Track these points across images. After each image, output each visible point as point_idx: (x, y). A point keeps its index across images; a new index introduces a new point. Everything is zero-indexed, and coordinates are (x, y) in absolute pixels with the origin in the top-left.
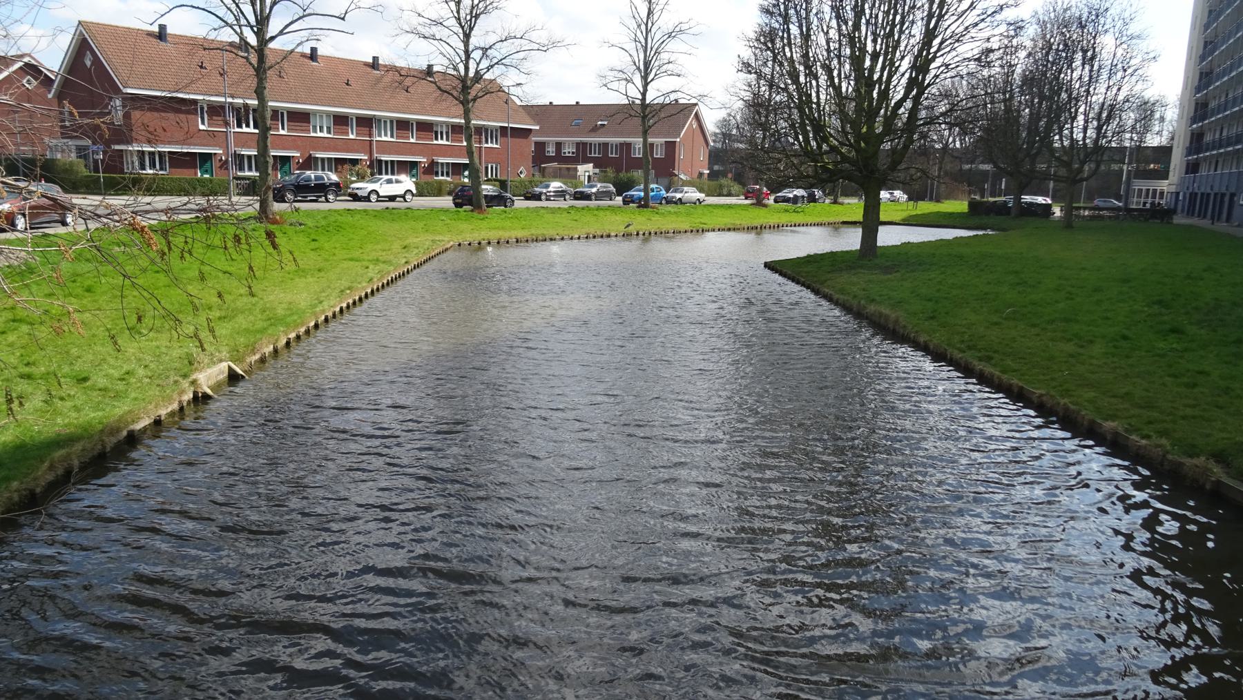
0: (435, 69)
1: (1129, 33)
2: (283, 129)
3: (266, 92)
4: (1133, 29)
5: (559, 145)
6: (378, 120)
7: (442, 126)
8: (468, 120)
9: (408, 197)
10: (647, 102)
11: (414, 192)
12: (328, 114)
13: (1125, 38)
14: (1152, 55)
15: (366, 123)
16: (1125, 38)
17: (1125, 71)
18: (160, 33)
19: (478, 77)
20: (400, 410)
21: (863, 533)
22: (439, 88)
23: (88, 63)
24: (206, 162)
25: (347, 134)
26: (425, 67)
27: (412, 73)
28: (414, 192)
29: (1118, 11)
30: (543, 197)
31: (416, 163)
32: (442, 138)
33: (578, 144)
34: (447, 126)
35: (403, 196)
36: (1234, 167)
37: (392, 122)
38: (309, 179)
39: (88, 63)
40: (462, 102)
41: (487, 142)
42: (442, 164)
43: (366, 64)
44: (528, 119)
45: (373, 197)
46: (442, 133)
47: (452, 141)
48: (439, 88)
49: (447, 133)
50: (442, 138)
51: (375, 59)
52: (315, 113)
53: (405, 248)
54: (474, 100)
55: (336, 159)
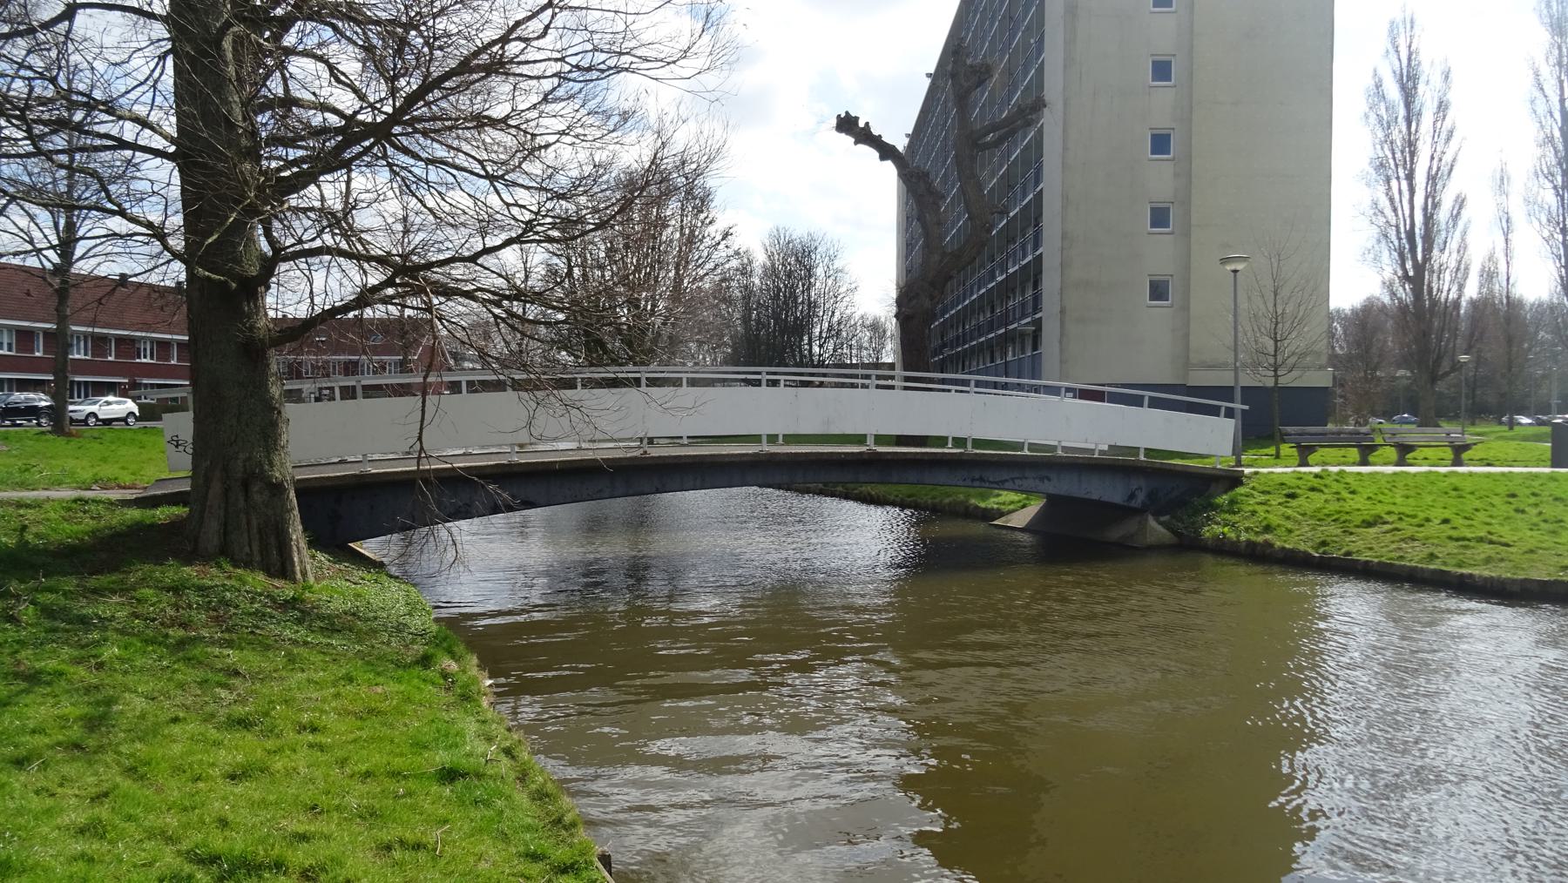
1: (835, 267)
4: (838, 264)
7: (145, 343)
9: (131, 420)
11: (138, 414)
13: (831, 272)
14: (853, 286)
16: (831, 272)
17: (836, 297)
21: (643, 620)
28: (138, 414)
29: (825, 249)
34: (152, 343)
35: (124, 420)
36: (981, 363)
38: (120, 596)
42: (79, 383)
45: (92, 421)
46: (145, 349)
49: (152, 350)
53: (7, 438)
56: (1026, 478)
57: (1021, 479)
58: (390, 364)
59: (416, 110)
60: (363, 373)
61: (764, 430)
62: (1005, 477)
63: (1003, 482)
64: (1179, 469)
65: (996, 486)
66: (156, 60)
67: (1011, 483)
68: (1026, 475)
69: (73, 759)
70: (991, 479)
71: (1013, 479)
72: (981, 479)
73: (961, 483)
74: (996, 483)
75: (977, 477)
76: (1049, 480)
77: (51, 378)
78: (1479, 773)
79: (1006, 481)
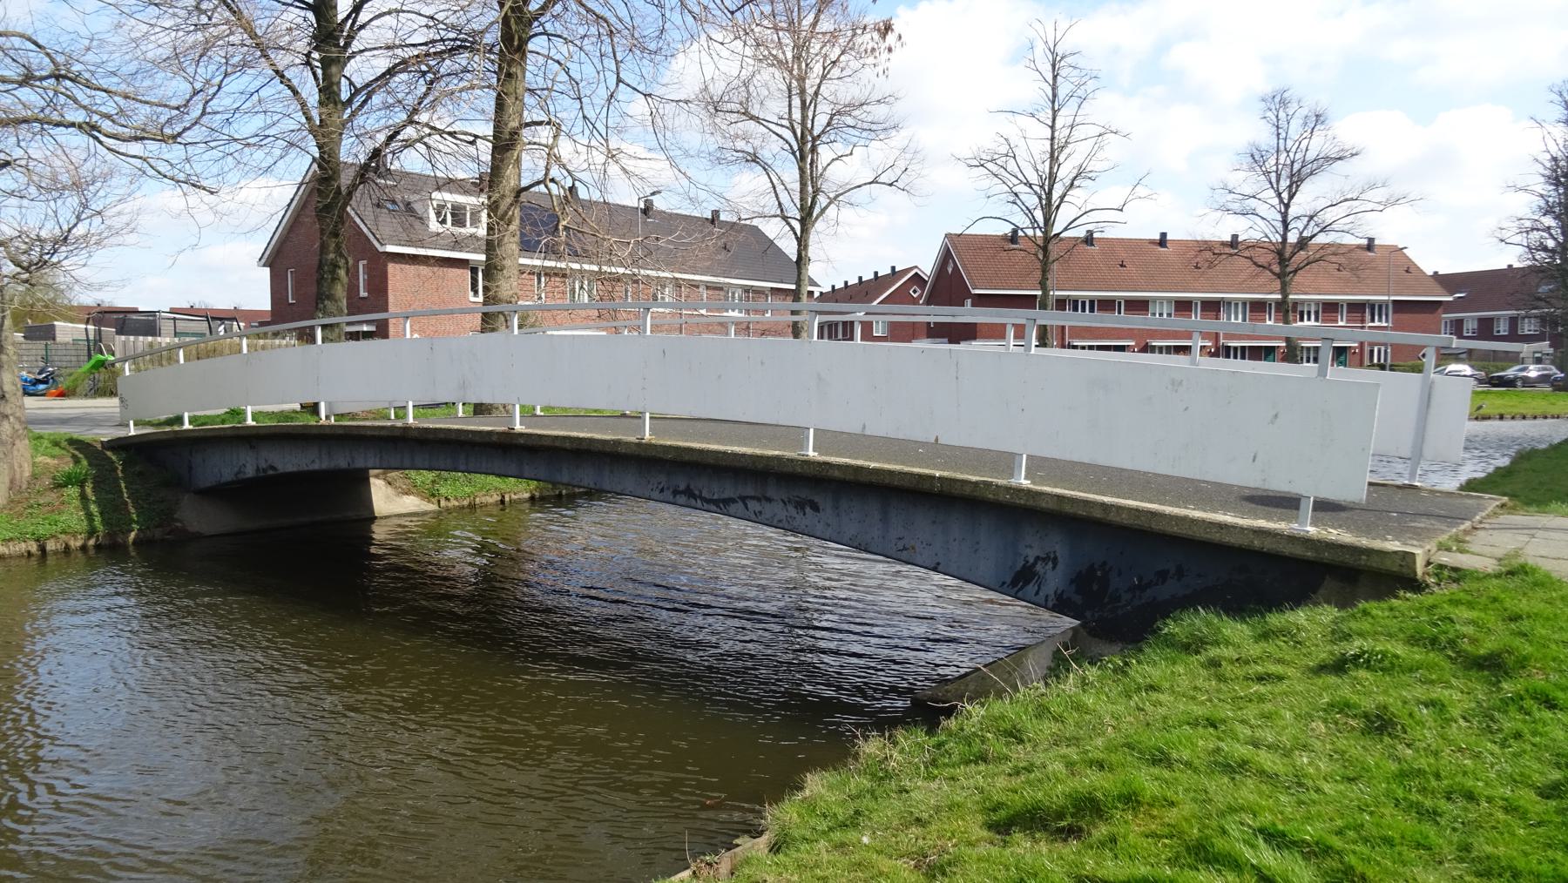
0: (723, 217)
2: (1270, 319)
3: (1048, 283)
5: (1513, 321)
6: (1228, 303)
8: (1285, 295)
10: (1056, 230)
12: (1169, 300)
15: (1212, 307)
18: (1161, 240)
19: (1303, 243)
20: (953, 645)
22: (1255, 263)
23: (950, 270)
24: (1270, 354)
25: (1336, 321)
26: (1229, 239)
27: (1261, 245)
30: (1519, 383)
31: (1273, 348)
32: (1309, 319)
33: (1481, 320)
37: (1244, 304)
39: (950, 270)
40: (1279, 276)
41: (1373, 320)
42: (1308, 349)
43: (1152, 242)
44: (1439, 289)
46: (1309, 313)
47: (1323, 321)
48: (1255, 263)
49: (1317, 313)
50: (1309, 319)
51: (1235, 237)
52: (1155, 300)
54: (1295, 271)
55: (1175, 347)
56: (769, 500)
57: (759, 500)
58: (1236, 304)
59: (22, 472)
60: (1451, 321)
61: (1310, 487)
62: (729, 493)
63: (727, 502)
64: (1125, 519)
65: (713, 508)
66: (751, 151)
67: (740, 505)
68: (771, 493)
69: (518, 161)
70: (705, 494)
71: (744, 499)
72: (689, 493)
73: (655, 494)
74: (715, 502)
75: (682, 487)
76: (815, 508)
77: (1133, 344)
78: (84, 156)
79: (733, 500)
